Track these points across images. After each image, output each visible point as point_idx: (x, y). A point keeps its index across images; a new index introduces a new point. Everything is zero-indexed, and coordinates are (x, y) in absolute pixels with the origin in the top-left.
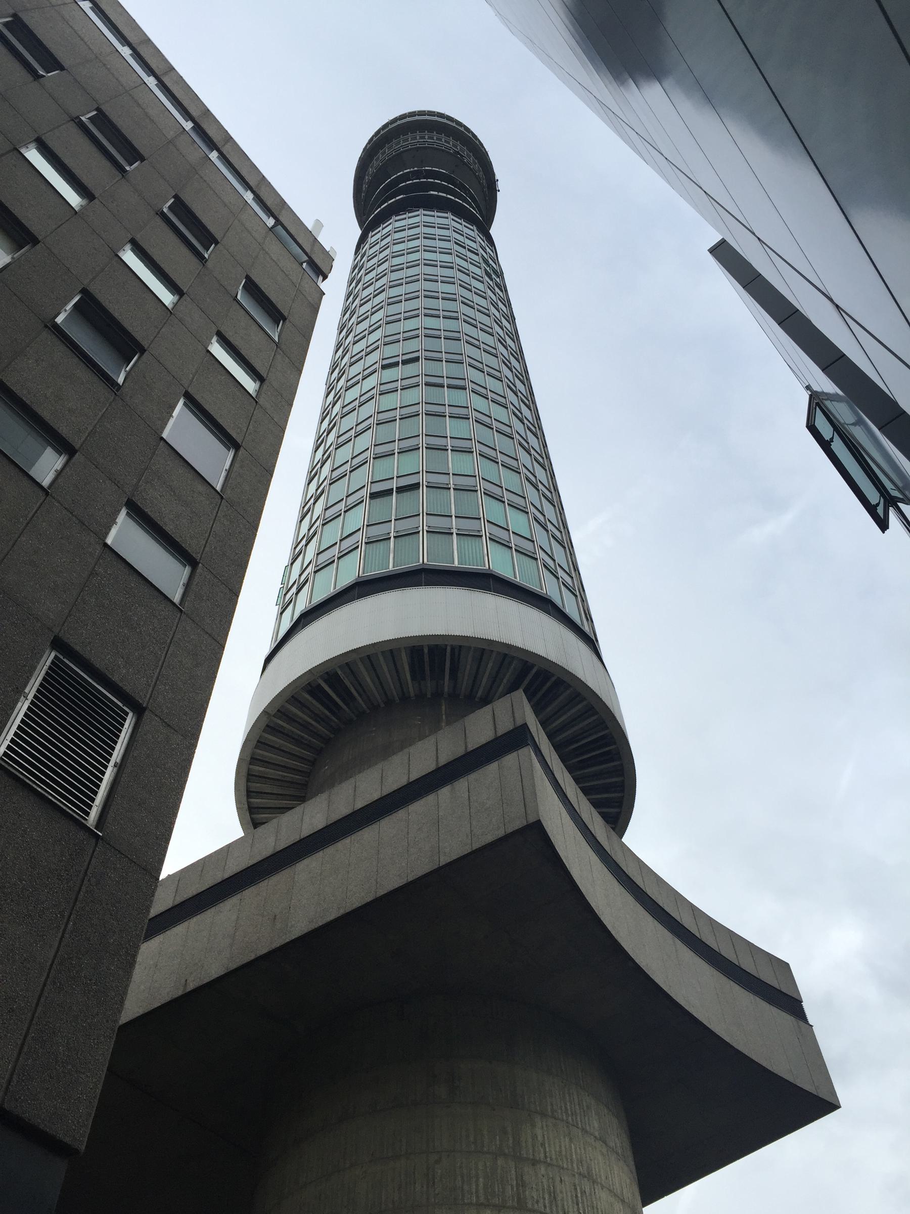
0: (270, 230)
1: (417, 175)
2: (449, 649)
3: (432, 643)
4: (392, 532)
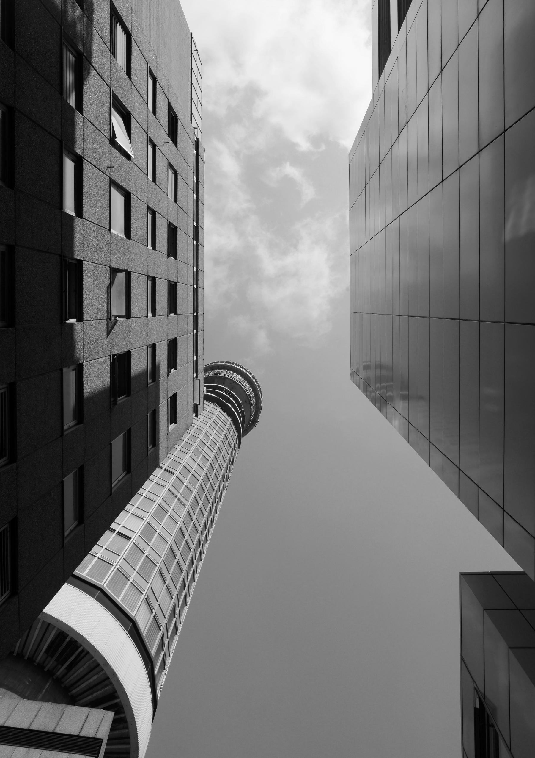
0: (193, 379)
1: (227, 392)
2: (81, 648)
3: (76, 638)
4: (99, 554)
